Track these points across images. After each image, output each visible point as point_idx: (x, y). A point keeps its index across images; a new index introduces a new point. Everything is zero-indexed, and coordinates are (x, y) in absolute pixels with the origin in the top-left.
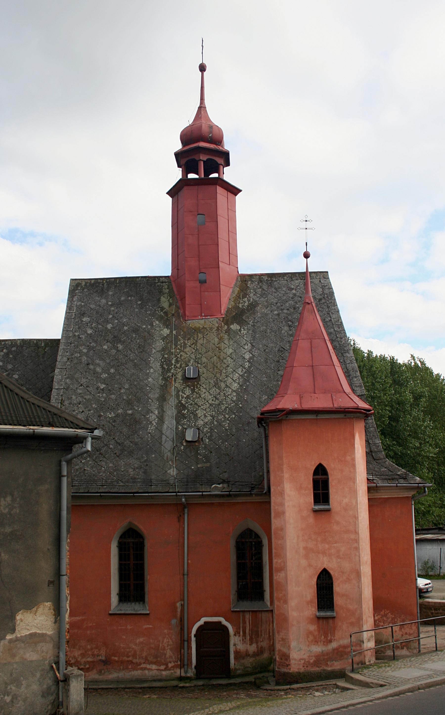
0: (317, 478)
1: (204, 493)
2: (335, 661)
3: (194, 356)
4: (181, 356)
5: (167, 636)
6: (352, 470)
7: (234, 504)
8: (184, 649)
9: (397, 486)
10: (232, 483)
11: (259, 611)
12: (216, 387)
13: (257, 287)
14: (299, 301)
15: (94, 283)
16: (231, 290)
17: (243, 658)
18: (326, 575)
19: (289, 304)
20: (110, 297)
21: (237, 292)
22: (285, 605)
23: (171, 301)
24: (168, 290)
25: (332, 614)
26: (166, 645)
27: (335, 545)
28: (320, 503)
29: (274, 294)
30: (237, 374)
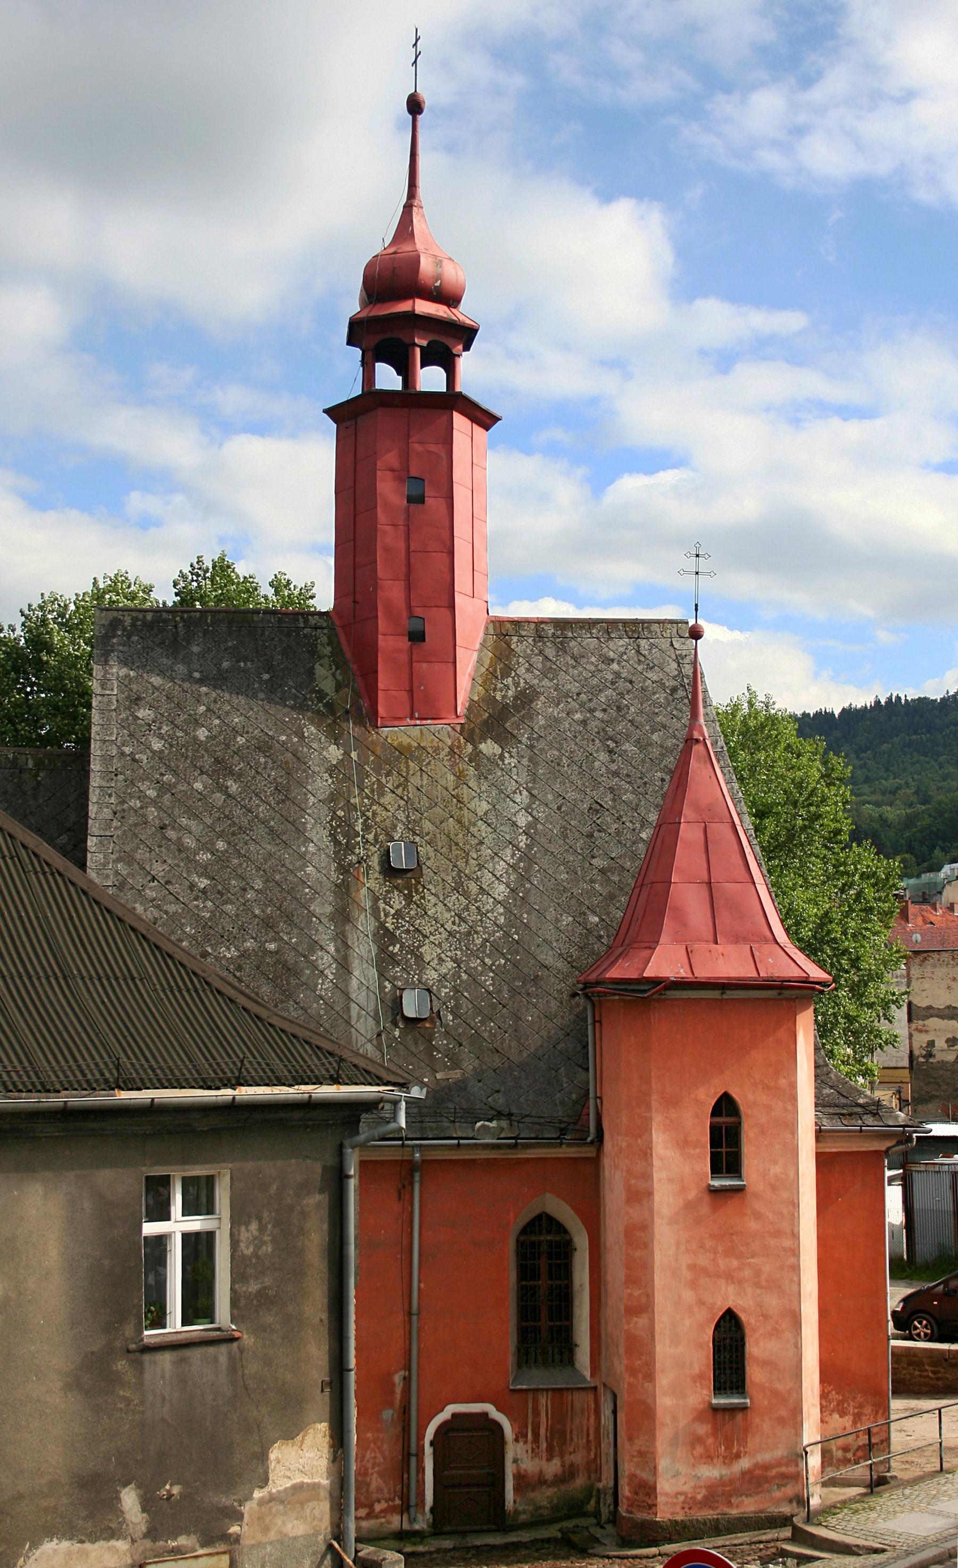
0: (718, 1123)
1: (461, 1141)
2: (747, 1496)
3: (403, 815)
4: (374, 814)
5: (372, 1445)
6: (789, 1107)
7: (520, 1162)
8: (408, 1472)
9: (861, 1131)
10: (517, 1119)
11: (568, 1389)
12: (458, 892)
13: (532, 650)
14: (628, 692)
15: (153, 622)
16: (475, 656)
17: (533, 1490)
18: (730, 1321)
19: (606, 696)
20: (195, 659)
21: (488, 662)
22: (647, 1384)
23: (339, 678)
24: (329, 649)
25: (743, 1401)
26: (369, 1465)
27: (752, 1260)
28: (722, 1173)
29: (571, 670)
30: (502, 863)
